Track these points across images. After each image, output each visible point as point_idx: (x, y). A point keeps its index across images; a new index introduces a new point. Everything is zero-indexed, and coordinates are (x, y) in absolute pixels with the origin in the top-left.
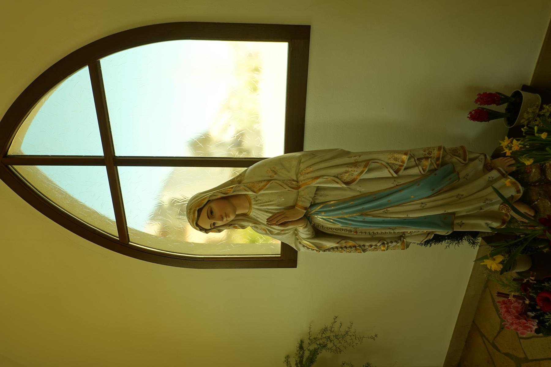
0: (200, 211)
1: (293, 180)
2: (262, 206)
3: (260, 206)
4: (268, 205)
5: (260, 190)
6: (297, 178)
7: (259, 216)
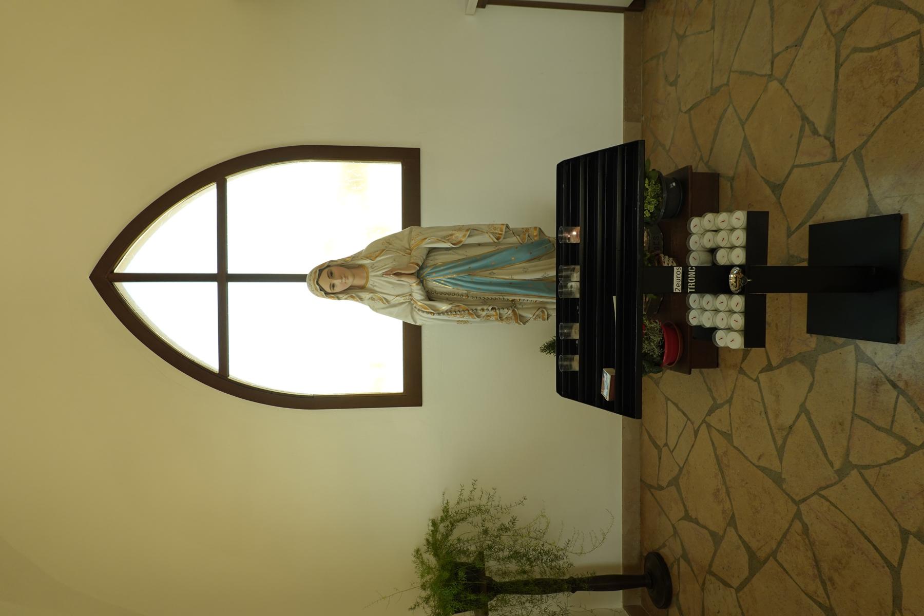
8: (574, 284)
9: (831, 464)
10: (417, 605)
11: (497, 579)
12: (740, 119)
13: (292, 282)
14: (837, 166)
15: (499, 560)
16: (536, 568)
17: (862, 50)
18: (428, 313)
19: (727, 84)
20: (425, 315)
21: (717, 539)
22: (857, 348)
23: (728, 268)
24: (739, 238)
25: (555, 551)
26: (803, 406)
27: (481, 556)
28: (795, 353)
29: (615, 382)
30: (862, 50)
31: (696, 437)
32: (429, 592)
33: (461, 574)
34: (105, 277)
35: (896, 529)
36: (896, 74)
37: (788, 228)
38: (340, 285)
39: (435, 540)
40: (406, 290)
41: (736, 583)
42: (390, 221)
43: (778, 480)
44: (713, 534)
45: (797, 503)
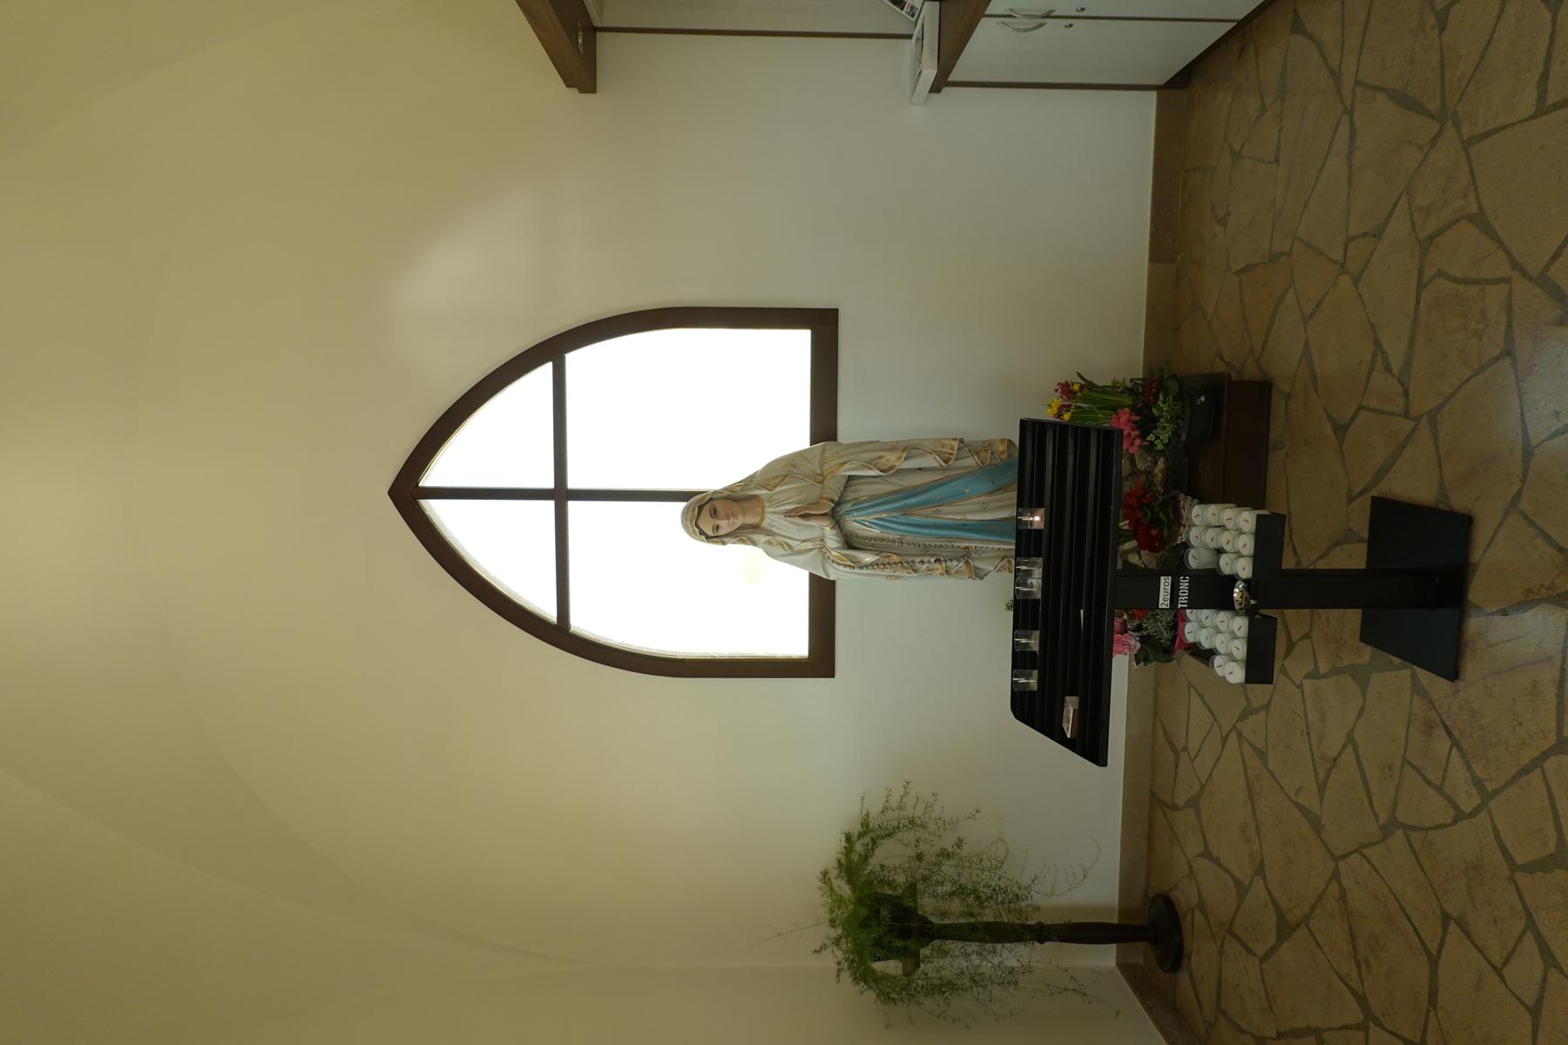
0: (701, 508)
8: (1036, 581)
9: (1376, 816)
10: (824, 947)
11: (935, 920)
12: (1302, 313)
13: (654, 484)
14: (1409, 425)
15: (935, 896)
16: (988, 912)
17: (1448, 277)
19: (1289, 254)
21: (1241, 889)
22: (1414, 675)
23: (1232, 580)
24: (1246, 544)
25: (1016, 890)
26: (1350, 735)
27: (912, 889)
28: (1346, 662)
29: (1081, 714)
30: (1448, 277)
31: (1223, 746)
32: (839, 931)
33: (884, 912)
34: (408, 494)
35: (1438, 911)
36: (1481, 326)
37: (1350, 491)
38: (725, 526)
39: (850, 861)
40: (816, 534)
41: (1260, 949)
42: (795, 435)
43: (1316, 825)
44: (1237, 883)
45: (1337, 859)
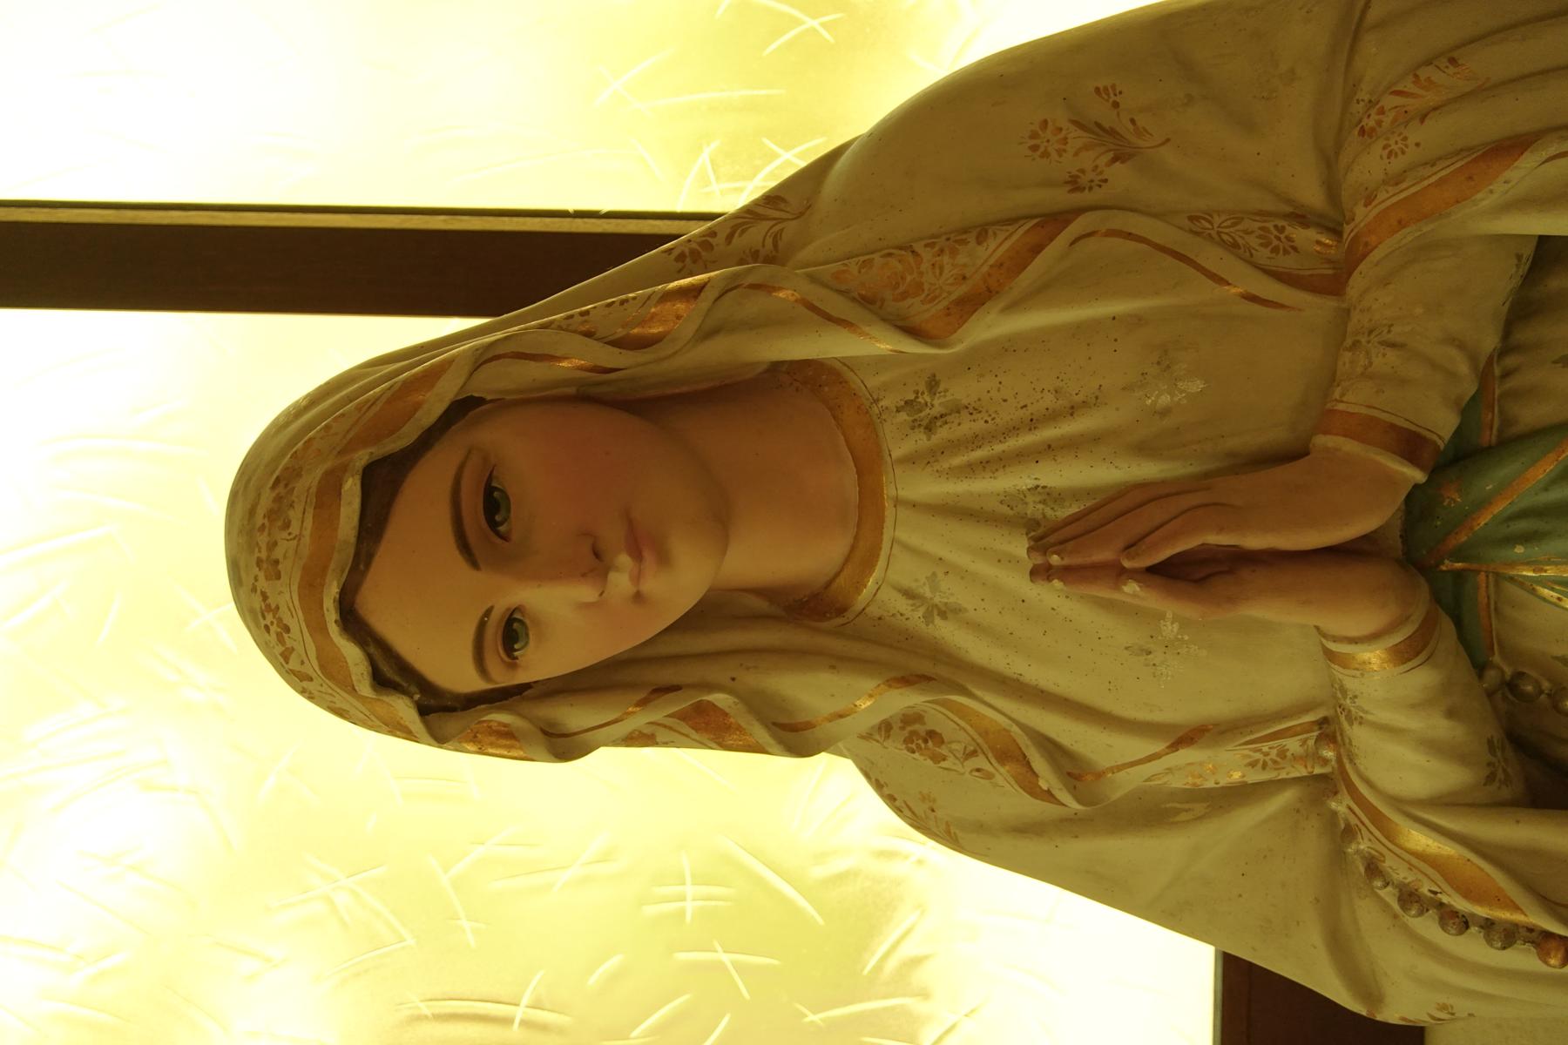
0: (384, 482)
1: (1301, 217)
2: (985, 465)
3: (971, 469)
4: (1050, 450)
5: (969, 305)
6: (1332, 190)
7: (953, 592)
18: (1509, 936)
20: (1472, 946)
